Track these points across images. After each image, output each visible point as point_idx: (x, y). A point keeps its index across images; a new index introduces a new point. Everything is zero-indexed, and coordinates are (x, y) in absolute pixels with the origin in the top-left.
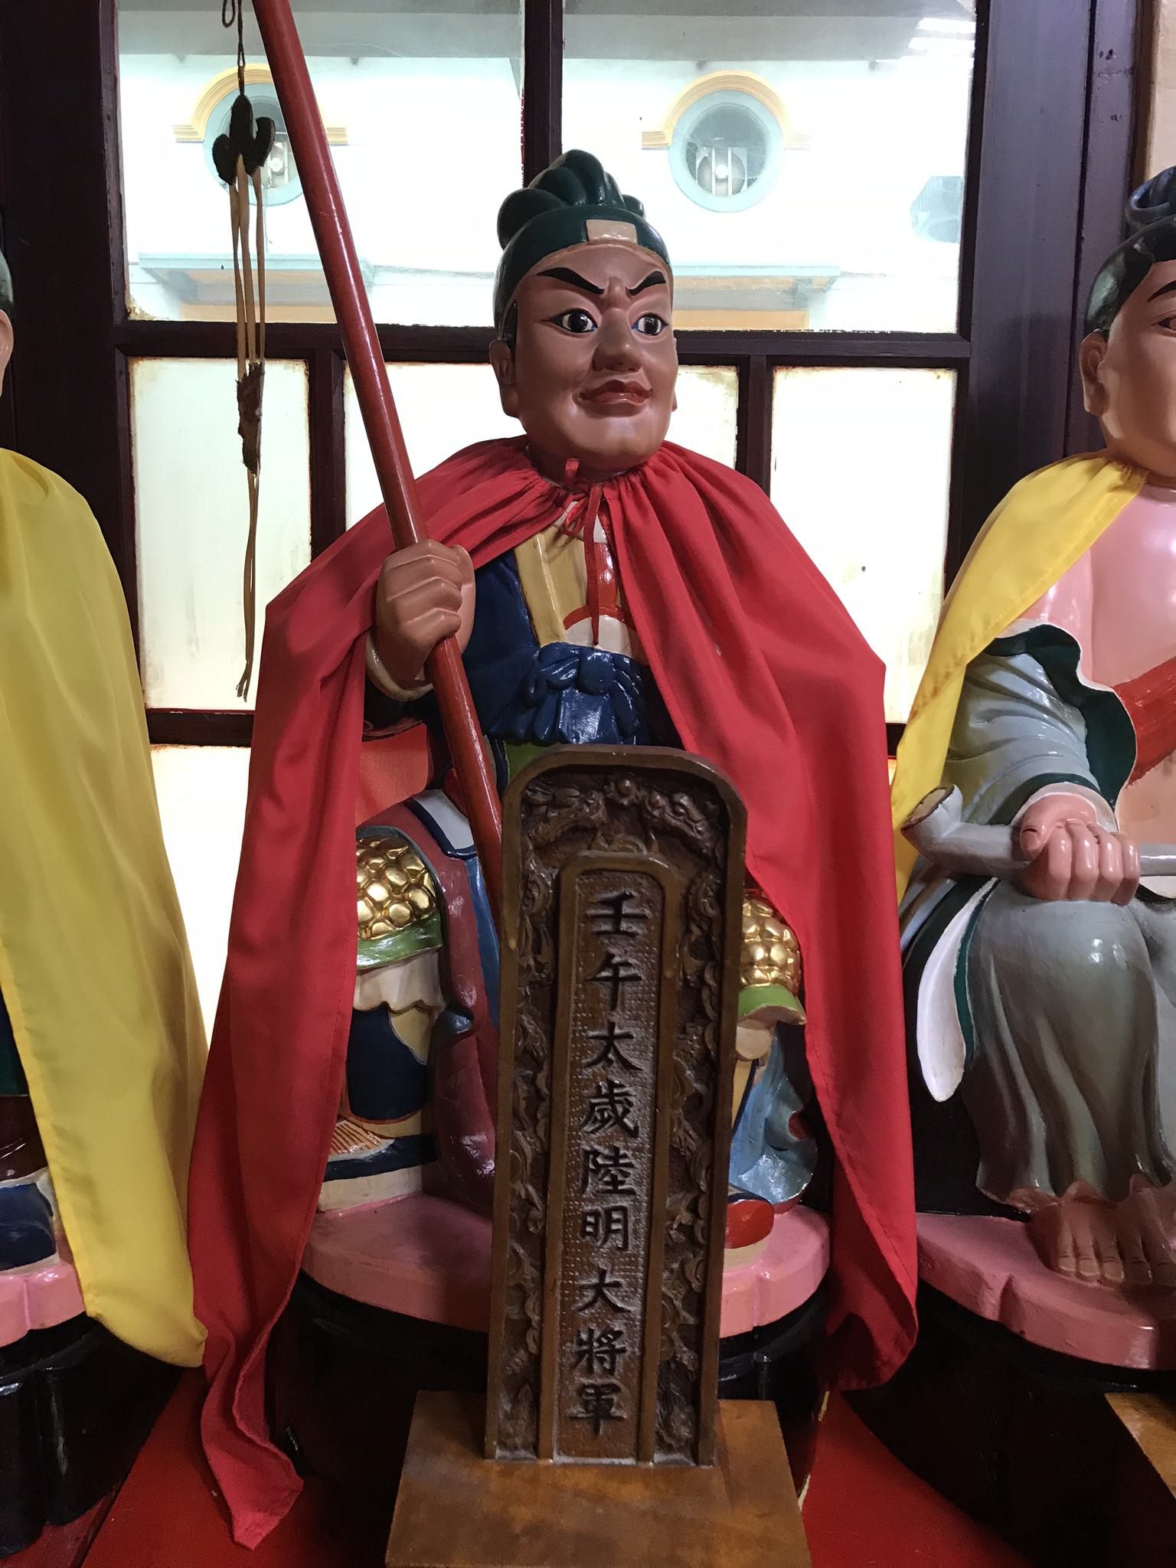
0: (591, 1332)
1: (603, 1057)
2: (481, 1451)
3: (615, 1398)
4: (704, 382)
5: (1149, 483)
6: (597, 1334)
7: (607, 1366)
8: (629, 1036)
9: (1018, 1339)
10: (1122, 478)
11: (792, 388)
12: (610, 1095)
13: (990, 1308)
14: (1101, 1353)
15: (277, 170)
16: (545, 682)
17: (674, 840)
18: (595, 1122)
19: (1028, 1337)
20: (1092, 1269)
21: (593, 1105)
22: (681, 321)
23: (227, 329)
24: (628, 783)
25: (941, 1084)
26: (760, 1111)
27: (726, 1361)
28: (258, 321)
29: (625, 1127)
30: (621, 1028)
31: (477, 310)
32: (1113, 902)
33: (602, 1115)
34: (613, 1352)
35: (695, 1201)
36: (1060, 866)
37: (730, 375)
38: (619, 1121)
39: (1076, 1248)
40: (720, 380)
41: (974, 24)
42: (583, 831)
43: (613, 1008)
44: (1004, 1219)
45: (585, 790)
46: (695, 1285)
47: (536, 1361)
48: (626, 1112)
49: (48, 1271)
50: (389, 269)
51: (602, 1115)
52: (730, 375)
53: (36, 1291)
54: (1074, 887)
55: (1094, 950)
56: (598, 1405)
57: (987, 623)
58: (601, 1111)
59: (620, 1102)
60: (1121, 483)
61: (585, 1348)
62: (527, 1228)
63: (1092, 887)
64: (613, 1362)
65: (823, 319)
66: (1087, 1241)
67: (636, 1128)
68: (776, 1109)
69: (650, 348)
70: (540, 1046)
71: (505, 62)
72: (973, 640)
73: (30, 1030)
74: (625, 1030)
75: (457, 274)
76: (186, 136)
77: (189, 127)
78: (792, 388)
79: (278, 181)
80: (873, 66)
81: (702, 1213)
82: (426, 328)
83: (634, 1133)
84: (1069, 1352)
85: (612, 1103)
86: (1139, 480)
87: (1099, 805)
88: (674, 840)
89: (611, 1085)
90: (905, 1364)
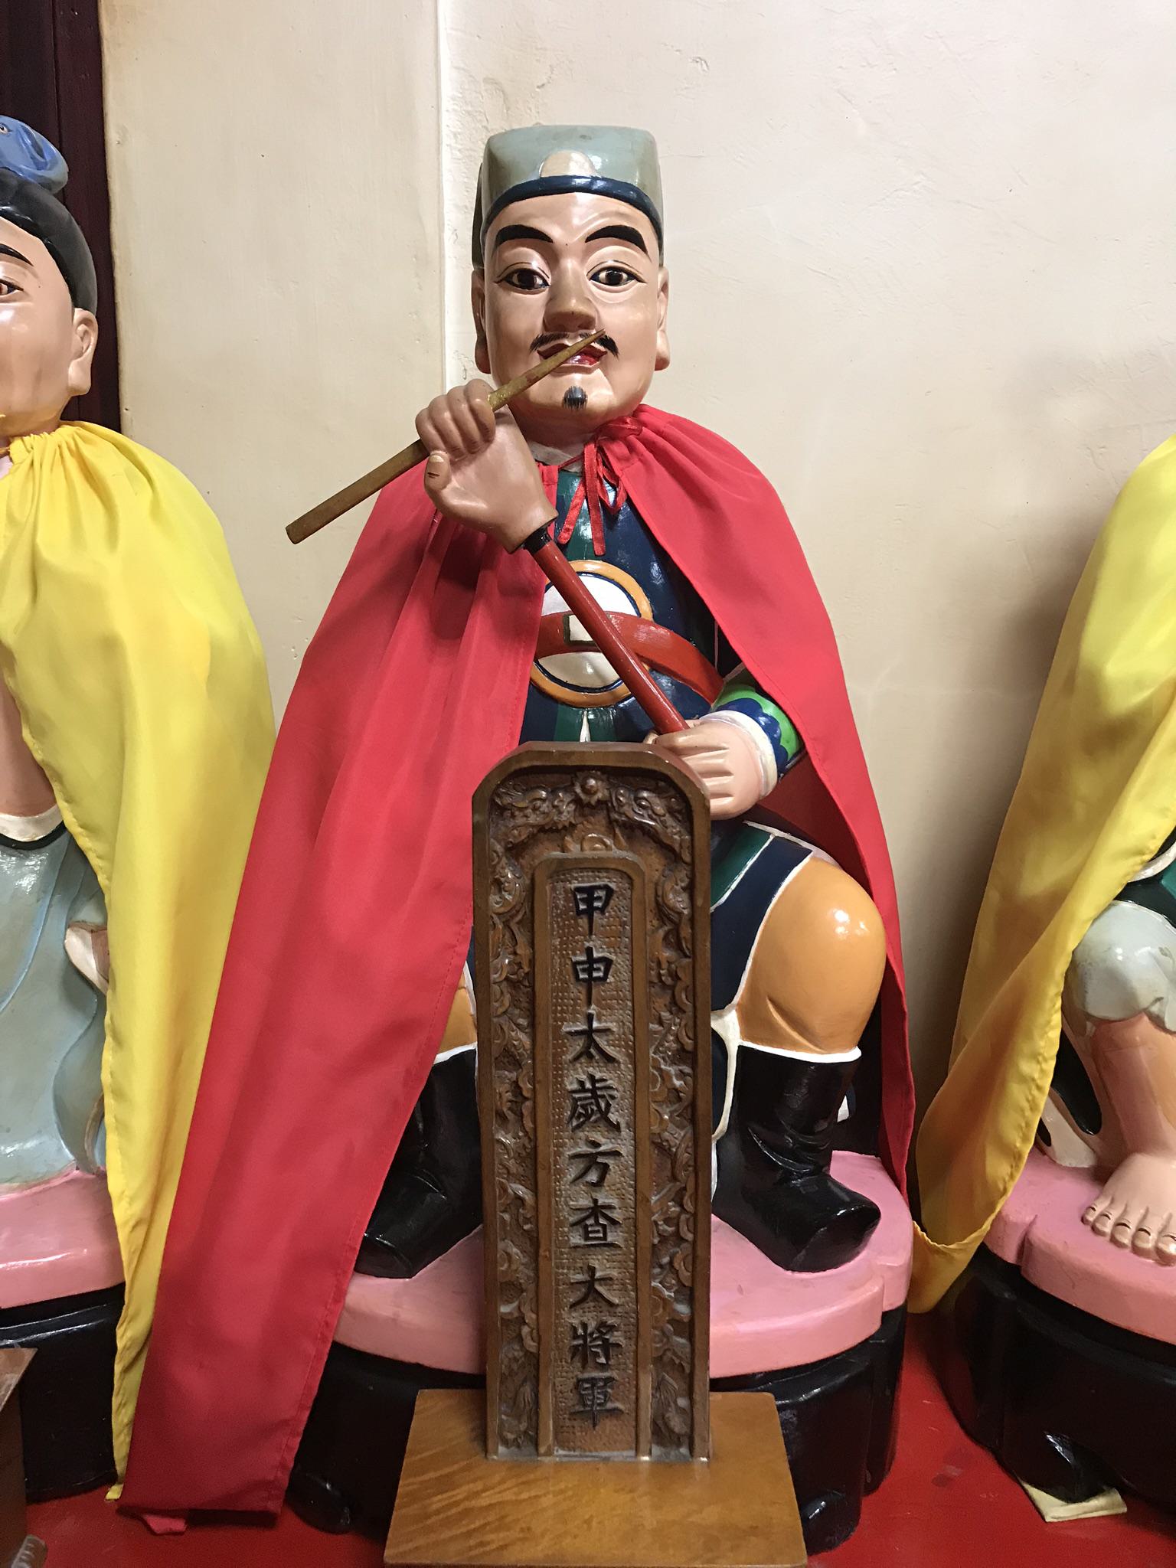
0: (585, 1326)
1: (586, 1054)
6: (589, 1330)
7: (603, 1360)
12: (594, 1090)
16: (547, 596)
17: (633, 831)
18: (578, 1118)
21: (576, 1100)
24: (592, 782)
27: (596, 345)
30: (599, 1020)
34: (607, 1347)
38: (604, 1115)
42: (554, 831)
43: (589, 1004)
45: (553, 792)
46: (685, 1275)
48: (608, 1105)
58: (584, 1107)
59: (603, 1097)
74: (603, 1025)
85: (595, 1097)
89: (592, 1078)
90: (542, 255)
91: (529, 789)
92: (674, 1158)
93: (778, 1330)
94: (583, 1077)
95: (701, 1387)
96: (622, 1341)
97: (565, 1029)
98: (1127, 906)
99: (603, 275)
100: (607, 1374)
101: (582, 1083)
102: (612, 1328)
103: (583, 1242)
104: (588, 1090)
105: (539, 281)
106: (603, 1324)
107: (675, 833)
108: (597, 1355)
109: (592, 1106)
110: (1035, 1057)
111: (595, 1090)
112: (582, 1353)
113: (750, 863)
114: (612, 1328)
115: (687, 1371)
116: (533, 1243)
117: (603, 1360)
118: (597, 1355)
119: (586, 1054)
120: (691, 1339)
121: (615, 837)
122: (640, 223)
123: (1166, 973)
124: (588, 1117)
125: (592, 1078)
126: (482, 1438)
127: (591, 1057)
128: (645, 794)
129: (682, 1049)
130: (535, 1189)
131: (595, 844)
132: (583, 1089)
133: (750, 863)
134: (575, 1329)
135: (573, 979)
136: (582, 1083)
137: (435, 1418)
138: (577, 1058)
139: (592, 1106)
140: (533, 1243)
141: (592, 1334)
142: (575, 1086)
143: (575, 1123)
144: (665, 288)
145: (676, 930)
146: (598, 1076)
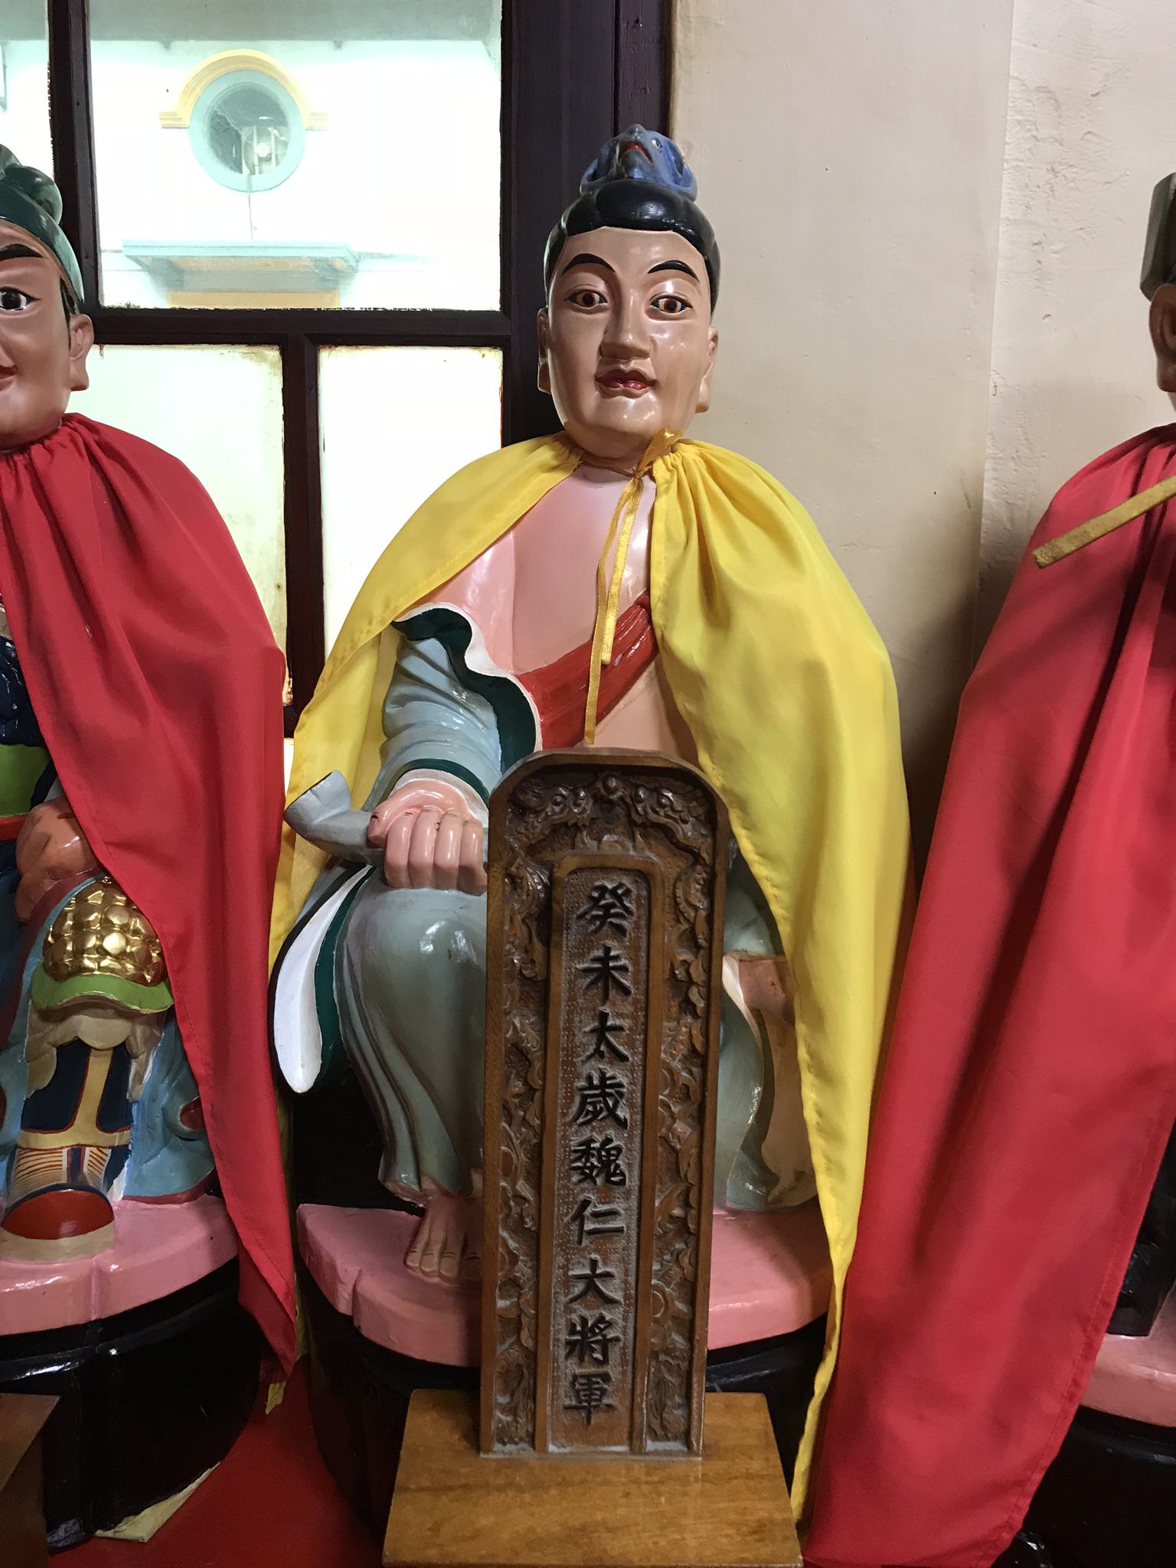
0: (584, 1321)
1: (597, 1051)
4: (247, 361)
5: (584, 463)
9: (357, 1332)
10: (556, 457)
11: (339, 368)
13: (343, 1306)
14: (418, 1349)
15: (264, 155)
19: (365, 1332)
20: (432, 1264)
25: (300, 1070)
26: (154, 1100)
29: (617, 1119)
31: (482, 292)
32: (459, 888)
35: (687, 1192)
36: (398, 855)
37: (273, 354)
38: (612, 1113)
39: (428, 1244)
40: (264, 359)
44: (404, 1213)
47: (532, 1356)
50: (372, 255)
52: (273, 354)
54: (414, 876)
56: (588, 1397)
57: (387, 606)
58: (594, 1104)
59: (610, 1095)
60: (555, 463)
61: (579, 1337)
62: (524, 1222)
63: (430, 873)
65: (355, 297)
66: (439, 1236)
68: (171, 1098)
69: (20, 326)
70: (531, 1040)
71: (477, 45)
72: (370, 623)
74: (618, 1022)
75: (385, 257)
76: (171, 123)
77: (174, 114)
78: (339, 368)
79: (265, 166)
82: (385, 311)
84: (390, 1346)
86: (575, 461)
87: (465, 791)
89: (603, 1074)
91: (528, 1050)
94: (575, 1318)
97: (571, 1273)
99: (662, 302)
100: (593, 1370)
103: (574, 1403)
104: (579, 1333)
106: (602, 1319)
108: (593, 1350)
109: (601, 1167)
112: (578, 1348)
114: (610, 1324)
116: (535, 1242)
118: (593, 1350)
119: (598, 1054)
120: (692, 1303)
121: (633, 839)
122: (695, 261)
123: (554, 469)
124: (596, 1113)
125: (603, 1074)
126: (475, 1438)
127: (602, 1055)
129: (693, 1050)
130: (538, 1188)
132: (591, 1086)
134: (574, 1325)
136: (590, 1078)
137: (426, 1427)
138: (589, 1058)
139: (601, 1167)
140: (535, 1242)
141: (592, 1330)
142: (583, 1083)
143: (581, 1120)
144: (715, 339)
145: (692, 933)
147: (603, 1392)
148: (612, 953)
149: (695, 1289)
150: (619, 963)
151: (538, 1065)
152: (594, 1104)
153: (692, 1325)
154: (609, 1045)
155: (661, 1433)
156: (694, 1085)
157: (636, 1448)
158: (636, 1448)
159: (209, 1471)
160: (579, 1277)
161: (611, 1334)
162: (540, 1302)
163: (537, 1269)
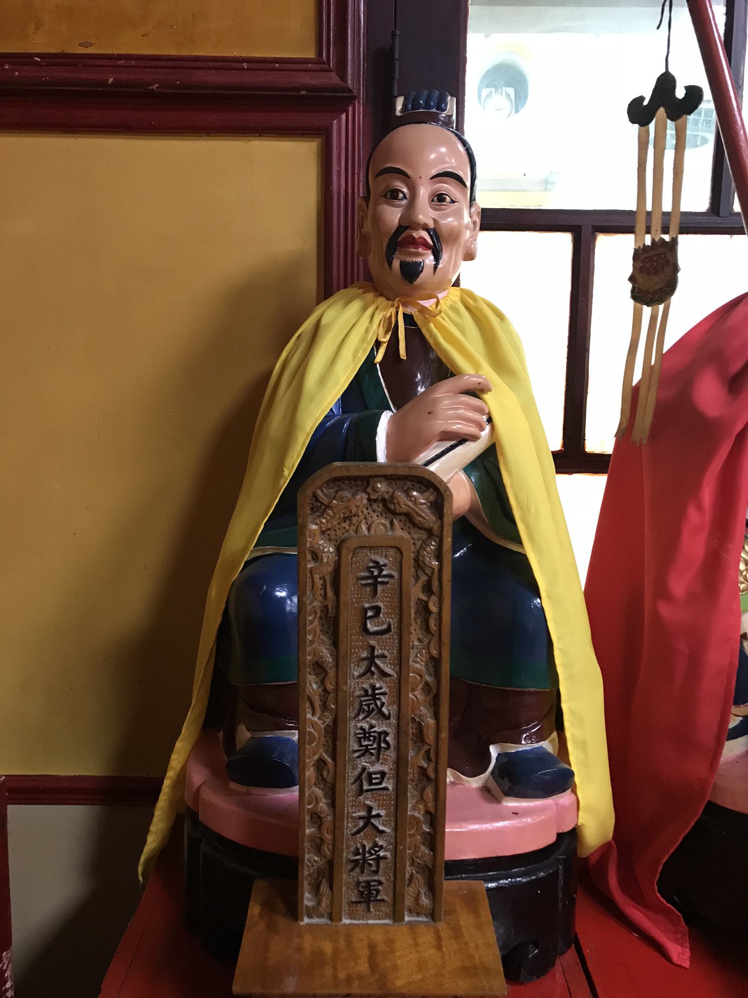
0: (364, 847)
1: (368, 671)
2: (293, 911)
3: (380, 888)
8: (384, 657)
12: (374, 694)
17: (409, 519)
22: (487, 199)
23: (629, 214)
28: (649, 208)
33: (369, 708)
34: (378, 859)
35: (428, 752)
41: (725, 8)
47: (331, 864)
48: (383, 704)
49: (565, 798)
51: (369, 708)
53: (560, 808)
55: (289, 596)
58: (368, 705)
59: (379, 699)
64: (378, 866)
67: (390, 714)
70: (327, 657)
73: (560, 650)
80: (487, 36)
81: (433, 758)
83: (388, 717)
88: (409, 519)
89: (374, 688)
92: (430, 688)
93: (332, 216)
94: (365, 686)
95: (441, 872)
96: (388, 854)
98: (664, 71)
100: (376, 878)
101: (366, 691)
102: (381, 847)
103: (357, 899)
105: (401, 195)
106: (376, 845)
107: (428, 517)
109: (370, 704)
110: (671, 135)
111: (373, 694)
113: (380, 373)
115: (434, 691)
117: (374, 868)
118: (370, 865)
127: (373, 673)
128: (415, 493)
130: (334, 759)
131: (378, 526)
132: (366, 695)
133: (380, 373)
135: (357, 625)
139: (370, 704)
141: (369, 852)
146: (378, 685)
147: (378, 891)
148: (374, 813)
149: (436, 819)
150: (381, 691)
151: (332, 673)
152: (368, 705)
153: (434, 839)
154: (377, 667)
155: (416, 910)
156: (433, 685)
157: (397, 917)
158: (397, 917)
159: (152, 842)
160: (361, 818)
161: (382, 854)
162: (336, 828)
163: (333, 805)
